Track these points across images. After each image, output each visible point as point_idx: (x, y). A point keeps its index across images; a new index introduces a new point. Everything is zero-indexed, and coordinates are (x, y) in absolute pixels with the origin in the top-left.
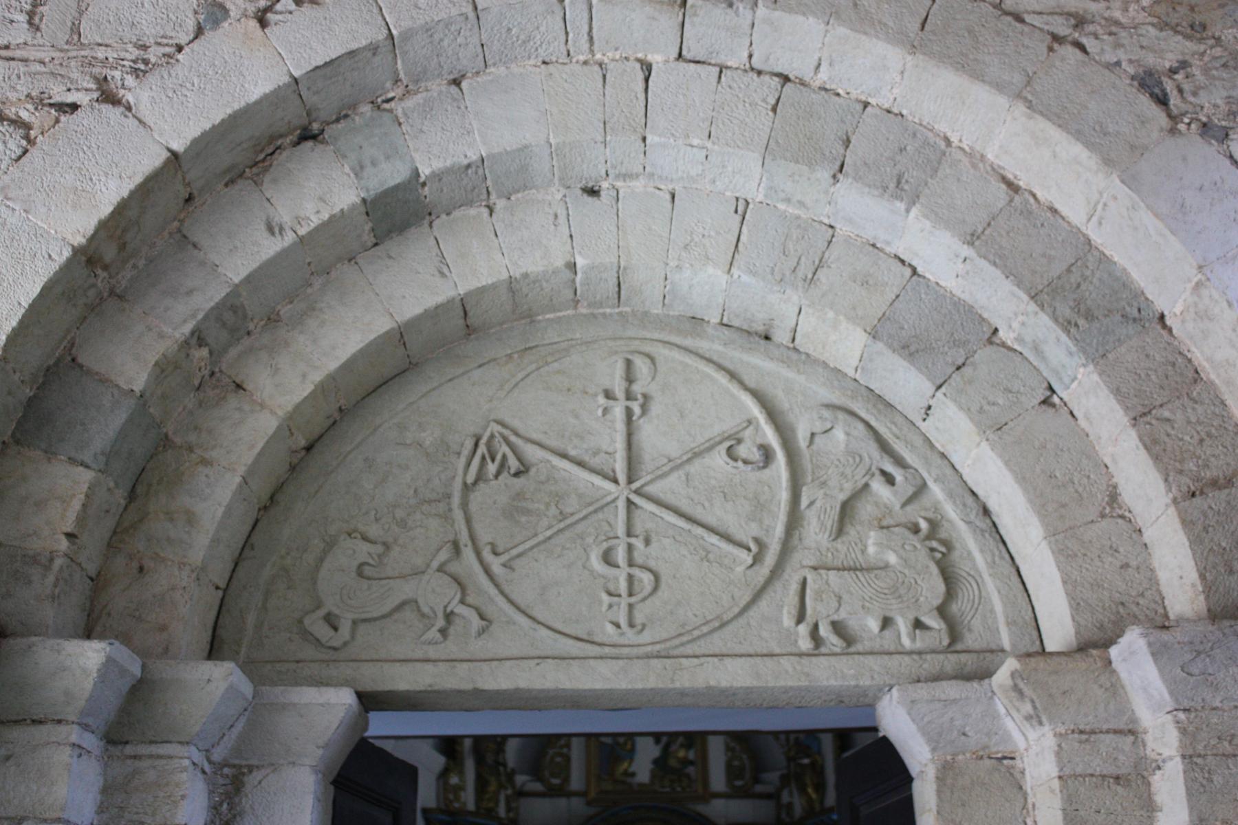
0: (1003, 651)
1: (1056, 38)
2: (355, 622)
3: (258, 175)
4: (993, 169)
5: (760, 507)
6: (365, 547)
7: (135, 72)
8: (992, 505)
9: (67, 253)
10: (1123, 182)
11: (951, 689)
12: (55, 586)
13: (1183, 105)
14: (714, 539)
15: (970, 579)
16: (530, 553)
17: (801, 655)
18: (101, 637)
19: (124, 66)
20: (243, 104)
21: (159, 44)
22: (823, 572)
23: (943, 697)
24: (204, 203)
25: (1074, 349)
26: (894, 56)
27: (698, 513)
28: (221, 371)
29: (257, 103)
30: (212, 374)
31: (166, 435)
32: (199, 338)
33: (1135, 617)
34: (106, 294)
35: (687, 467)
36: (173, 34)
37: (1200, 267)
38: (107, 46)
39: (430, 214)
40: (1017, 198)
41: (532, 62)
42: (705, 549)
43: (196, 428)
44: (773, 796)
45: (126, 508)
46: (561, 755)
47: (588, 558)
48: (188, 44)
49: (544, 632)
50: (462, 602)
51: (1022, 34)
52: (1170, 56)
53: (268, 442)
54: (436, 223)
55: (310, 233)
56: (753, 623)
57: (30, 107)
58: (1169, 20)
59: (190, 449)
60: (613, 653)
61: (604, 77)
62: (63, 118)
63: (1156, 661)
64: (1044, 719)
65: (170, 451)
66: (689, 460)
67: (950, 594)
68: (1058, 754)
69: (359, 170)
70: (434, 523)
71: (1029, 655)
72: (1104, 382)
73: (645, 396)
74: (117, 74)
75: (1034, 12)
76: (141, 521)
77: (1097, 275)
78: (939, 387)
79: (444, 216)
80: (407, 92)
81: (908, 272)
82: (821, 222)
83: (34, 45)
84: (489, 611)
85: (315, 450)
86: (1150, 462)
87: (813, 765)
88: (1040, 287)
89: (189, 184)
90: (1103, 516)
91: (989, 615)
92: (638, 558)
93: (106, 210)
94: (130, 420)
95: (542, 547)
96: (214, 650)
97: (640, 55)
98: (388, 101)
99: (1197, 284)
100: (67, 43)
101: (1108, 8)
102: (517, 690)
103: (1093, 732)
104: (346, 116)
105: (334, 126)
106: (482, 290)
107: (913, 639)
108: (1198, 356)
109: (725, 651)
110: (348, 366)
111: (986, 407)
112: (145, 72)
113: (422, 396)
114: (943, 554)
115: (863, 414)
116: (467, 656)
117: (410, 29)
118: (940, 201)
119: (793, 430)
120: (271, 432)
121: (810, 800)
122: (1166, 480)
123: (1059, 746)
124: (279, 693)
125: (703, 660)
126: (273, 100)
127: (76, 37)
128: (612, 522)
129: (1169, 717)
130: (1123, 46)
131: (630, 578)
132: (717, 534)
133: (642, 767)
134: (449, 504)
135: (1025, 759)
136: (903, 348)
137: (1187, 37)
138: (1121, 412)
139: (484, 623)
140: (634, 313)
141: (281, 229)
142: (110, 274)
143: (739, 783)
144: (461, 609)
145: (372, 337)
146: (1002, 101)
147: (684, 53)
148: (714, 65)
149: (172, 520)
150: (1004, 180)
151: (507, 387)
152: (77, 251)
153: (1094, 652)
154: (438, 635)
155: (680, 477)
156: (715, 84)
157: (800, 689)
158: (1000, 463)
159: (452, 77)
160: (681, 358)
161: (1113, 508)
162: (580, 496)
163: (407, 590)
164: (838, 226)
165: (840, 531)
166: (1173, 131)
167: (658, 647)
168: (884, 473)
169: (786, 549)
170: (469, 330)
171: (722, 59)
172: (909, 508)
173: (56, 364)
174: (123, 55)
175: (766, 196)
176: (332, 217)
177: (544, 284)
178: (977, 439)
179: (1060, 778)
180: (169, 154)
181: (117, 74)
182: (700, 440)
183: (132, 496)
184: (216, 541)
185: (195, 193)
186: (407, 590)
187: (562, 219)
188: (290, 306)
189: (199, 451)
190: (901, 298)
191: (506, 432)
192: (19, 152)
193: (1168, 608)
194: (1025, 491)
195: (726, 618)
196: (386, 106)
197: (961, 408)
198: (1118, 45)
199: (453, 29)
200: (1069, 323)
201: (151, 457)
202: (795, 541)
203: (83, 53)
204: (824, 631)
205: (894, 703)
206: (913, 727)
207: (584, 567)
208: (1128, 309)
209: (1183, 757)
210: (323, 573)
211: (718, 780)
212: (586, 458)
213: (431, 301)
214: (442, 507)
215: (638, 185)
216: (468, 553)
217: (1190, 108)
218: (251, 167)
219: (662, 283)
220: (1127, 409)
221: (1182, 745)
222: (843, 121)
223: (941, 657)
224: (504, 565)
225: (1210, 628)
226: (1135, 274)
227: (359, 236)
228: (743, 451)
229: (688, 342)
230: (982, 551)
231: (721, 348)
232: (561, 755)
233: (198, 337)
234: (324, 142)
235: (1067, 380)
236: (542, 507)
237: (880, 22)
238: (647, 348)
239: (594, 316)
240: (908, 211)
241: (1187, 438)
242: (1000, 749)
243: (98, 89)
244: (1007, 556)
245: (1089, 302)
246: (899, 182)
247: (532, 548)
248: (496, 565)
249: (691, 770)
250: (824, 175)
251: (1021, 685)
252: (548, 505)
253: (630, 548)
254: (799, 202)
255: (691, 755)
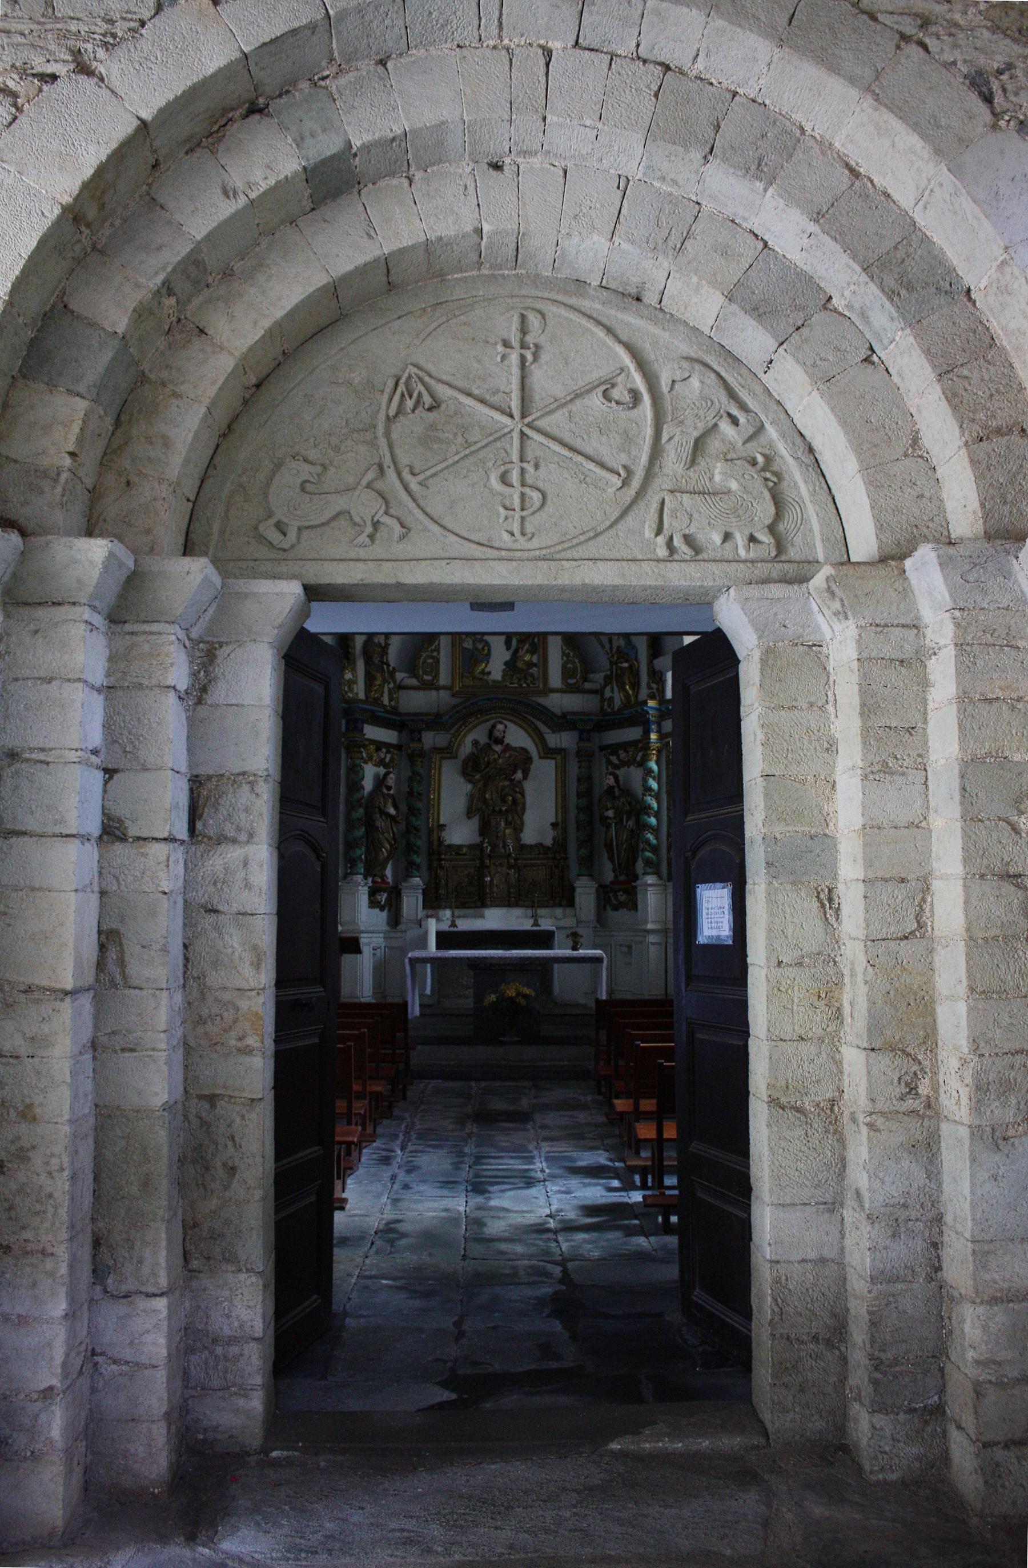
0: (817, 562)
1: (904, 37)
2: (300, 529)
3: (213, 144)
4: (839, 156)
5: (629, 440)
6: (307, 467)
7: (105, 45)
8: (816, 445)
9: (57, 211)
10: (949, 170)
11: (777, 590)
12: (63, 496)
13: (1005, 104)
14: (591, 466)
15: (795, 504)
16: (441, 475)
17: (658, 561)
18: (101, 535)
19: (95, 39)
20: (201, 77)
21: (124, 19)
22: (678, 494)
23: (770, 596)
24: (168, 170)
25: (895, 315)
26: (763, 48)
27: (579, 444)
28: (186, 318)
29: (214, 76)
30: (179, 320)
31: (143, 373)
32: (168, 288)
33: (925, 536)
34: (89, 250)
35: (570, 406)
36: (136, 9)
37: (1007, 248)
38: (78, 19)
39: (359, 183)
40: (857, 183)
41: (448, 45)
42: (583, 474)
43: (167, 366)
44: (599, 692)
45: (113, 434)
46: (433, 657)
47: (488, 479)
48: (150, 20)
49: (453, 538)
50: (386, 513)
51: (874, 31)
52: (999, 58)
53: (227, 379)
54: (364, 191)
55: (259, 197)
56: (621, 534)
57: (15, 76)
58: (1001, 25)
59: (163, 384)
60: (507, 554)
61: (511, 60)
62: (45, 88)
63: (942, 570)
64: (849, 614)
65: (147, 386)
66: (571, 400)
67: (778, 516)
68: (858, 642)
69: (300, 141)
70: (362, 449)
71: (842, 564)
72: (919, 344)
73: (537, 346)
74: (89, 46)
75: (886, 12)
76: (126, 443)
77: (919, 252)
78: (782, 344)
79: (370, 185)
80: (340, 71)
81: (761, 245)
82: (690, 199)
83: (14, 17)
84: (409, 521)
85: (263, 387)
86: (950, 412)
87: (631, 667)
88: (871, 261)
89: (155, 151)
90: (906, 455)
91: (808, 533)
92: (529, 480)
93: (89, 172)
94: (114, 359)
95: (451, 469)
96: (188, 549)
97: (542, 42)
98: (324, 78)
99: (1002, 262)
100: (43, 16)
101: (950, 10)
102: (431, 584)
103: (886, 626)
104: (288, 92)
105: (277, 101)
106: (402, 251)
107: (748, 550)
108: (994, 326)
109: (597, 556)
110: (291, 314)
111: (819, 362)
112: (114, 45)
113: (352, 343)
114: (775, 483)
115: (715, 367)
116: (390, 557)
117: (345, 10)
118: (793, 183)
119: (657, 378)
120: (229, 370)
121: (627, 696)
122: (961, 427)
123: (860, 635)
124: (243, 585)
125: (580, 562)
126: (225, 74)
127: (50, 11)
128: (508, 450)
129: (948, 614)
130: (960, 46)
131: (523, 495)
132: (593, 461)
133: (496, 668)
134: (374, 433)
135: (830, 647)
136: (754, 309)
137: (1015, 40)
138: (930, 369)
139: (404, 530)
140: (528, 275)
141: (235, 193)
142: (92, 231)
143: (571, 681)
144: (385, 519)
145: (311, 290)
146: (853, 93)
147: (581, 41)
148: (606, 53)
149: (151, 443)
150: (847, 165)
151: (422, 337)
152: (66, 209)
153: (893, 563)
154: (367, 539)
155: (564, 414)
156: (606, 70)
157: (656, 588)
158: (827, 410)
159: (379, 57)
160: (567, 315)
161: (914, 450)
162: (482, 428)
163: (340, 503)
164: (704, 203)
165: (693, 462)
166: (995, 127)
167: (544, 552)
168: (730, 415)
169: (649, 475)
170: (391, 286)
171: (613, 47)
172: (748, 445)
173: (52, 310)
174: (93, 28)
175: (644, 174)
176: (278, 183)
177: (455, 248)
178: (810, 389)
179: (858, 659)
180: (139, 122)
181: (89, 46)
182: (581, 383)
183: (118, 423)
184: (187, 460)
185: (161, 159)
186: (340, 503)
187: (471, 190)
188: (242, 263)
189: (171, 386)
190: (753, 267)
191: (421, 374)
192: (9, 119)
193: (951, 531)
194: (846, 433)
195: (599, 529)
196: (322, 83)
197: (798, 362)
198: (955, 46)
199: (381, 11)
200: (893, 292)
201: (132, 391)
202: (657, 469)
203: (58, 26)
204: (677, 542)
205: (731, 599)
206: (745, 620)
207: (485, 486)
208: (941, 282)
209: (956, 645)
210: (273, 488)
211: (555, 679)
212: (488, 397)
213: (361, 259)
214: (369, 435)
215: (536, 161)
216: (391, 474)
217: (1010, 106)
218: (207, 138)
219: (554, 249)
220: (934, 367)
221: (956, 636)
222: (715, 109)
223: (770, 565)
224: (420, 484)
225: (986, 545)
226: (950, 253)
227: (300, 201)
228: (615, 394)
229: (572, 301)
230: (806, 482)
231: (599, 307)
232: (433, 657)
233: (168, 288)
234: (269, 115)
235: (886, 341)
236: (451, 436)
237: (753, 16)
238: (539, 306)
239: (494, 276)
240: (765, 190)
241: (980, 393)
242: (810, 639)
243: (74, 61)
244: (825, 487)
245: (910, 276)
246: (759, 165)
247: (442, 470)
248: (413, 484)
249: (534, 670)
250: (696, 156)
251: (834, 587)
252: (455, 435)
253: (523, 471)
254: (672, 180)
255: (535, 659)
